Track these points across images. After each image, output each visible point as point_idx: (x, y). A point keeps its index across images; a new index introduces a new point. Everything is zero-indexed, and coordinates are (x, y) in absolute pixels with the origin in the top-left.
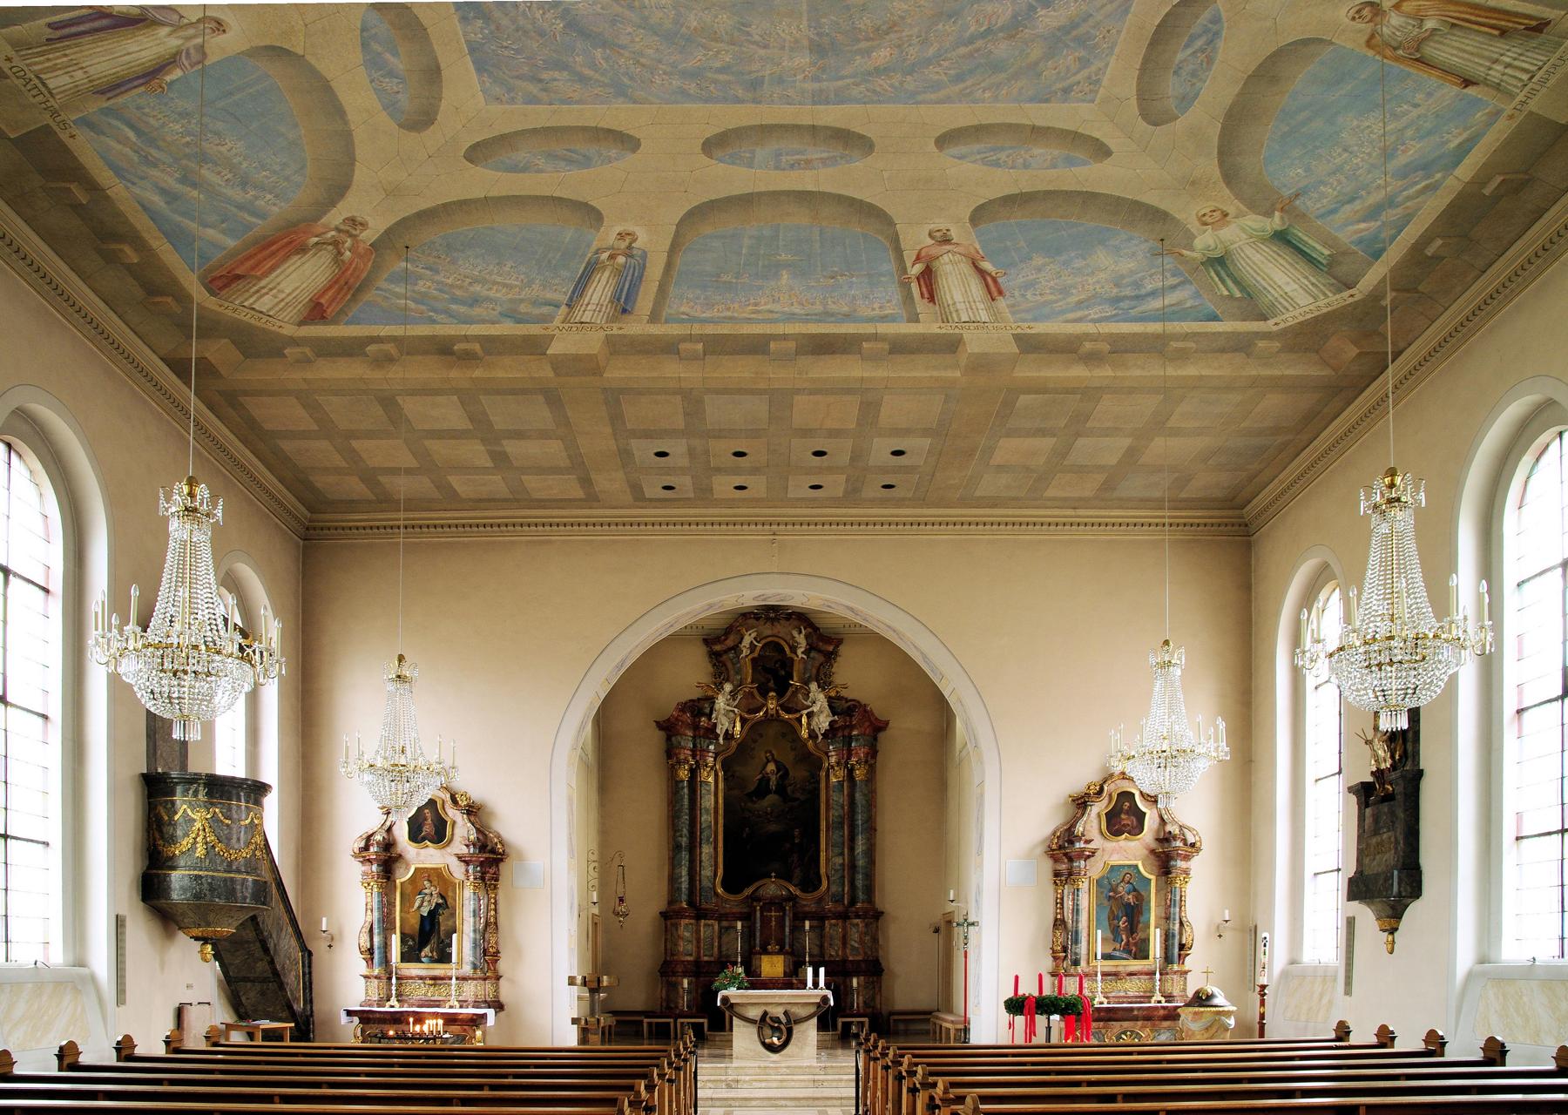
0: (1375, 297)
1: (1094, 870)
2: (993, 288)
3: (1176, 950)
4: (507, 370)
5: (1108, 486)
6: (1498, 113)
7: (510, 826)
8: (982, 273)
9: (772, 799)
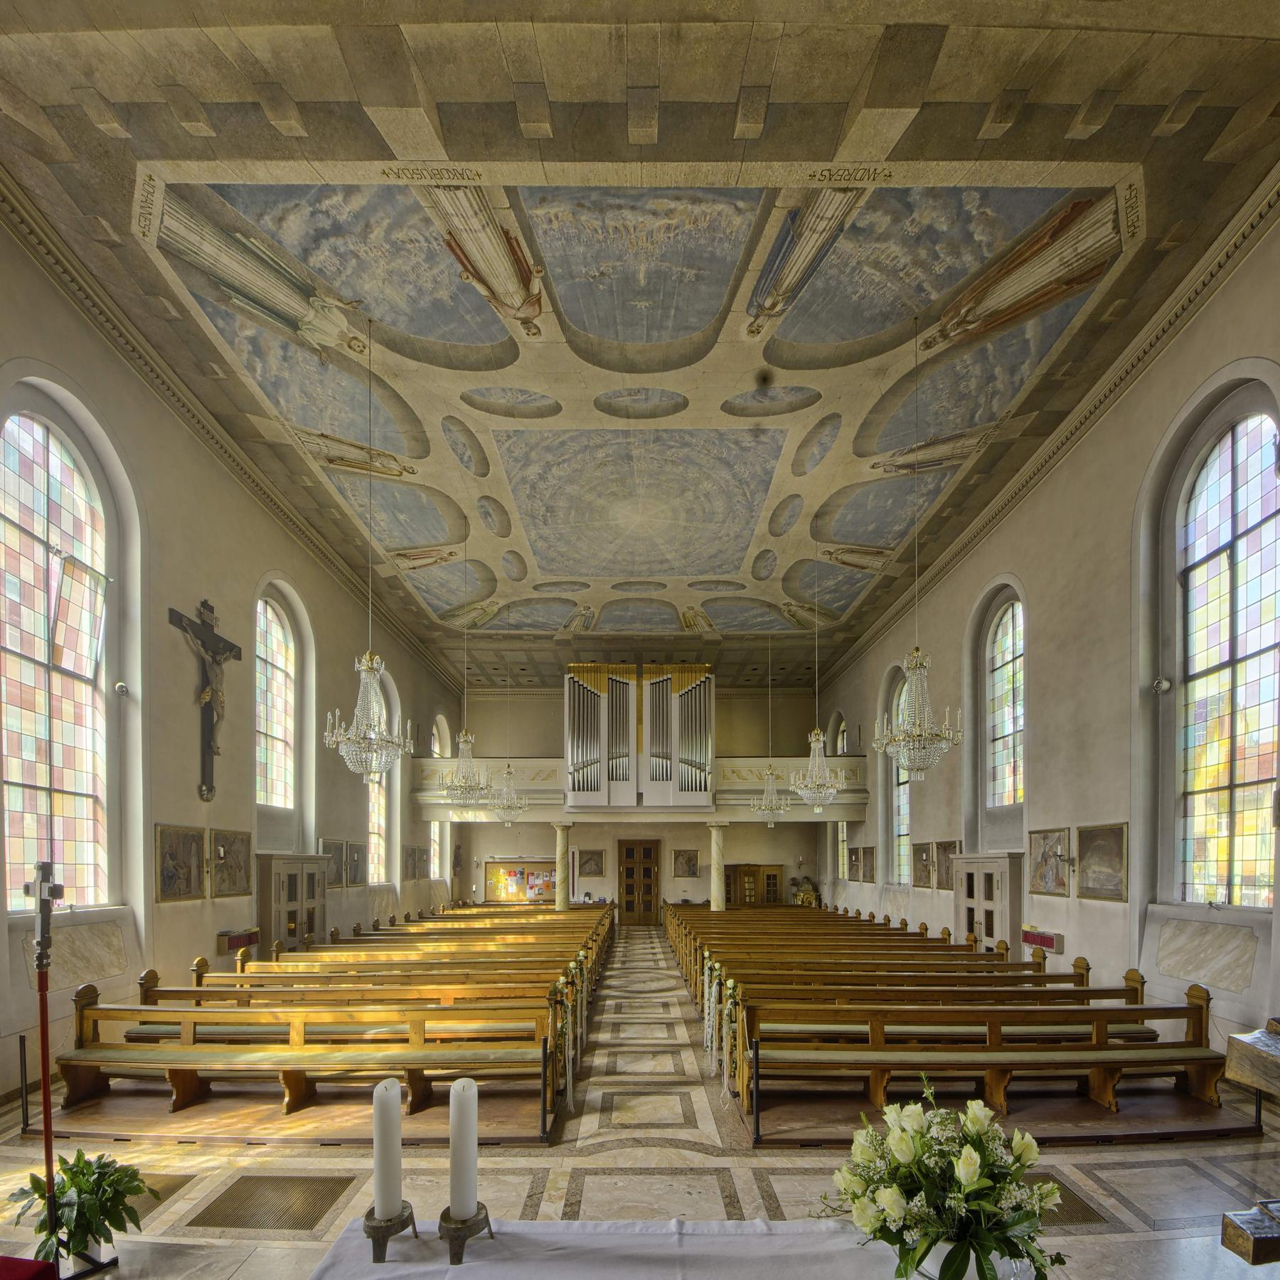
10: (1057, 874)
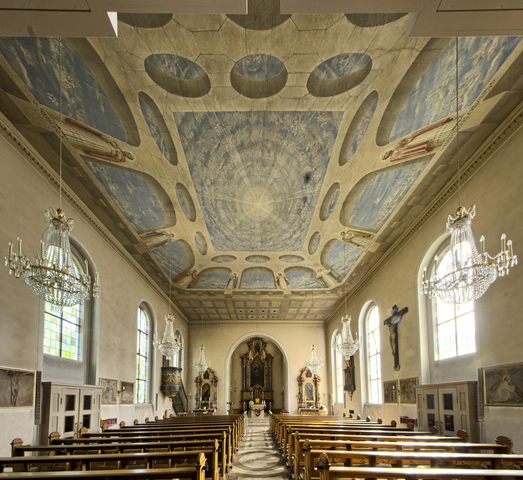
0: (344, 284)
1: (304, 384)
2: (288, 283)
3: (317, 399)
4: (219, 297)
5: (305, 317)
6: (363, 251)
7: (219, 375)
8: (286, 281)
9: (257, 370)
10: (113, 396)
